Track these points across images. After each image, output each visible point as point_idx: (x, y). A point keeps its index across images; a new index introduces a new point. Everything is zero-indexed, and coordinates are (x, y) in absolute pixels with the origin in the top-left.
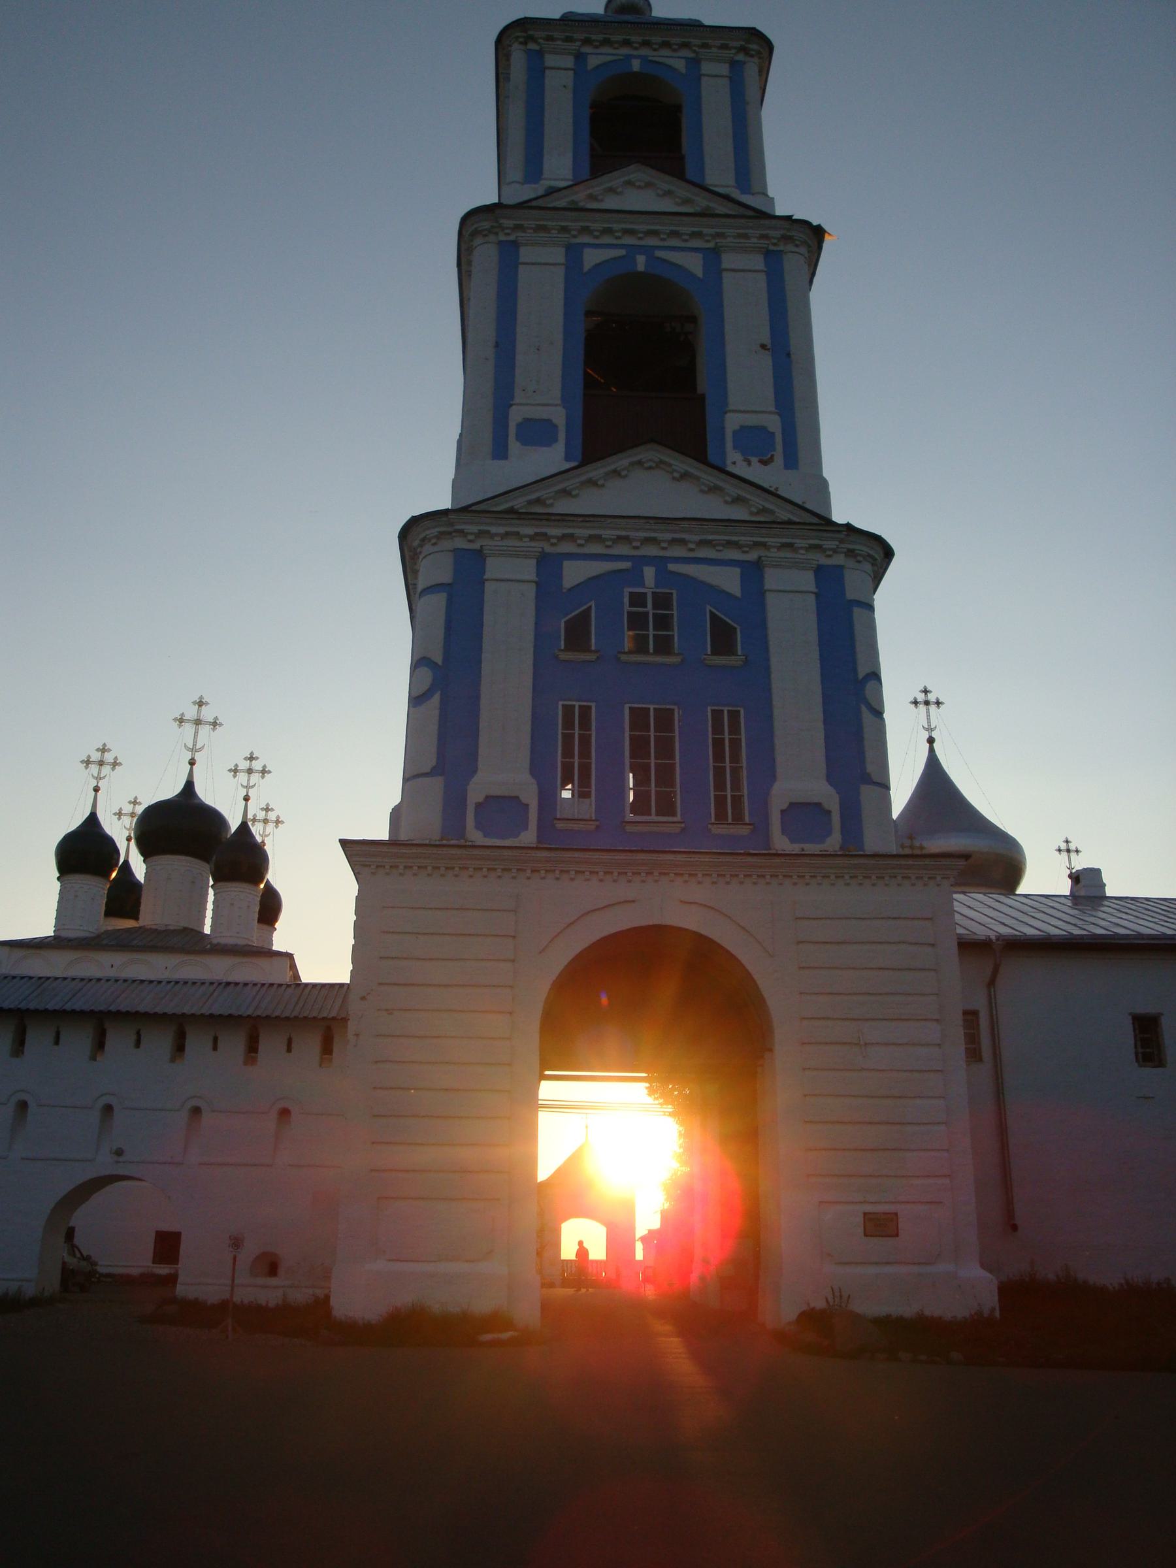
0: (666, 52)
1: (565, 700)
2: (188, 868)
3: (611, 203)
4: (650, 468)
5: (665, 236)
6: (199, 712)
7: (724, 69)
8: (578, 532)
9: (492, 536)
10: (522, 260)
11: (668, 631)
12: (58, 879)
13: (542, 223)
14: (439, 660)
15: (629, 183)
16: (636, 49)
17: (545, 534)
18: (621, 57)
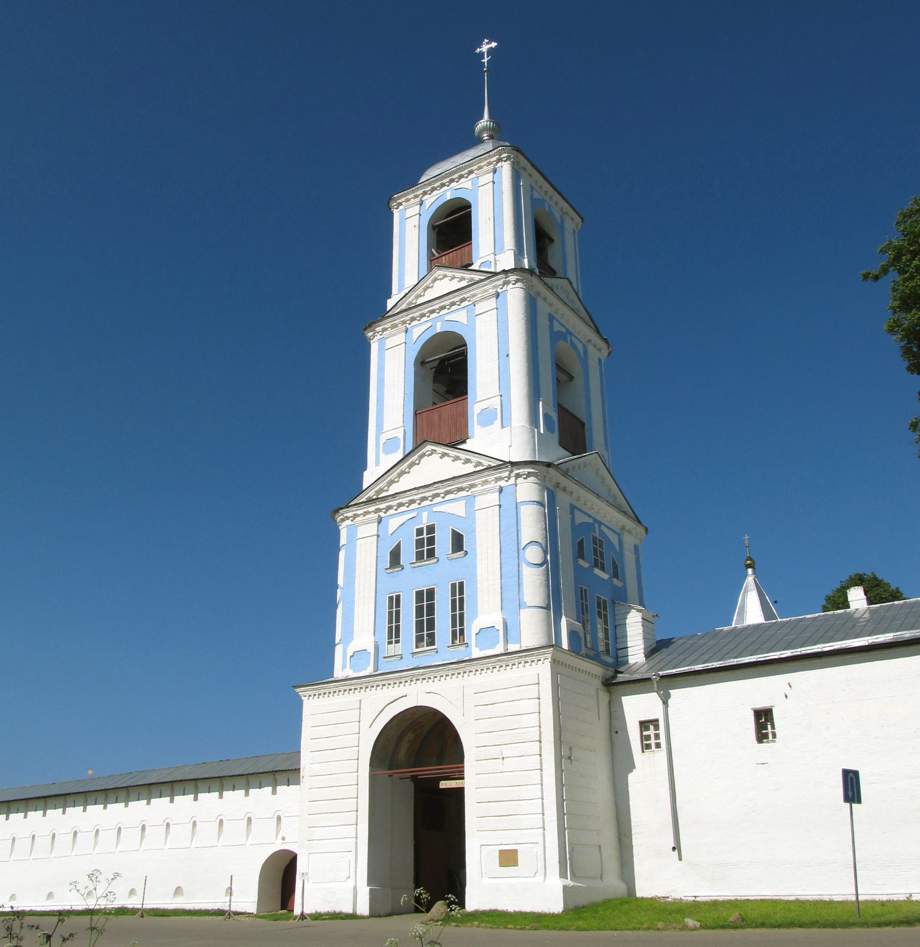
4: (430, 455)
8: (392, 503)
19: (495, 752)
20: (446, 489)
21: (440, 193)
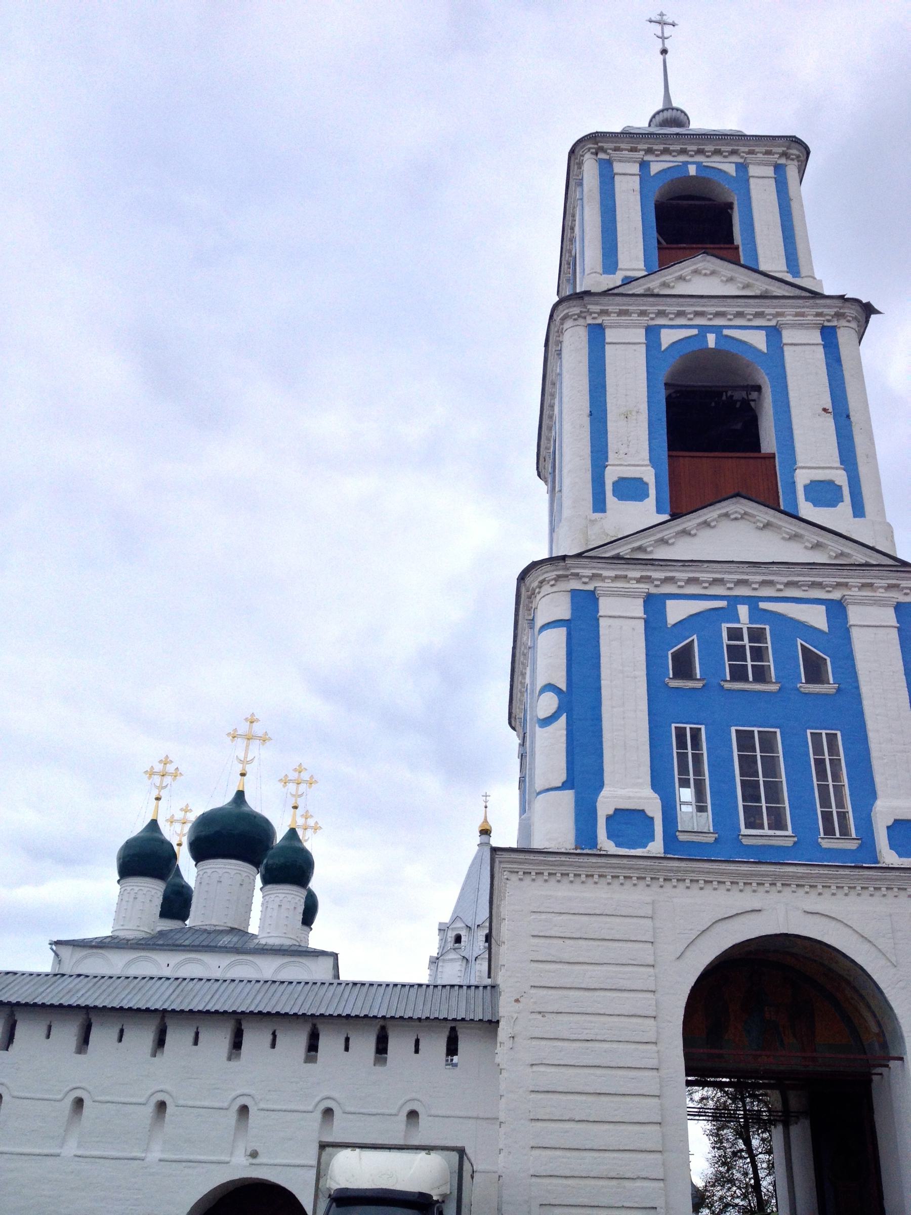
2: (238, 872)
3: (681, 289)
4: (736, 519)
6: (250, 728)
7: (770, 171)
10: (608, 340)
11: (763, 662)
12: (119, 882)
14: (563, 686)
15: (696, 272)
16: (692, 156)
17: (650, 577)
18: (680, 164)
20: (790, 579)
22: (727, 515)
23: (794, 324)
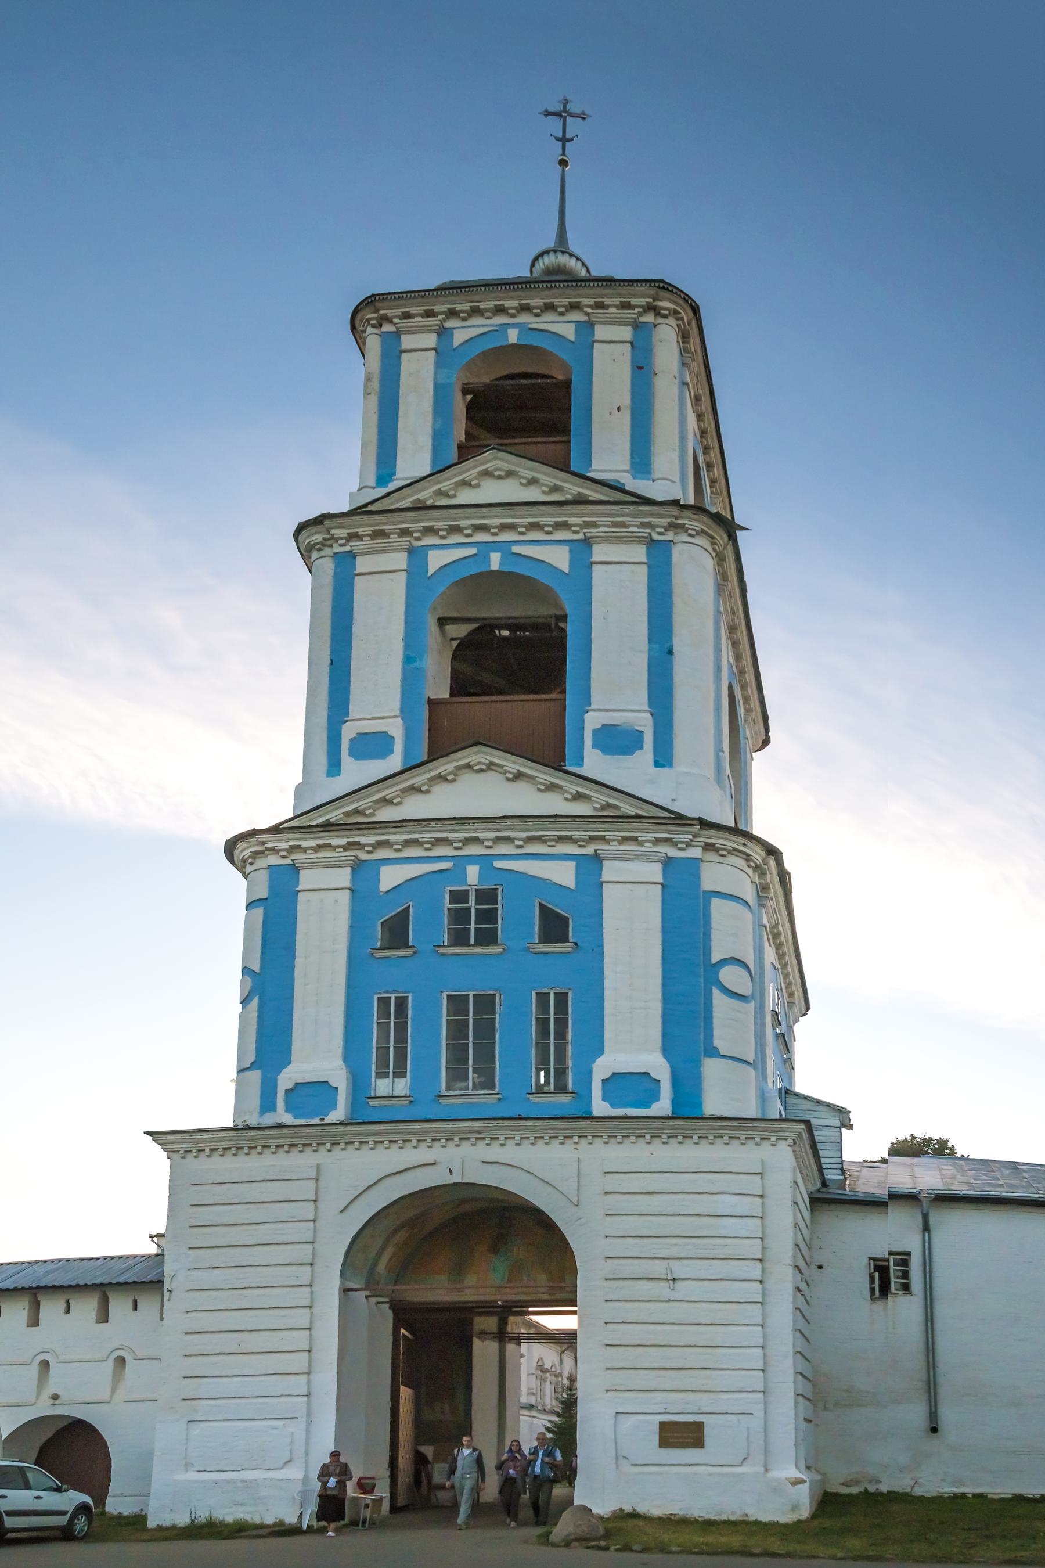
0: (550, 317)
1: (380, 993)
3: (465, 497)
4: (481, 770)
5: (550, 529)
8: (392, 838)
9: (305, 850)
13: (377, 528)
15: (487, 474)
16: (513, 316)
17: (358, 843)
19: (658, 1268)
20: (530, 834)
21: (491, 325)
22: (468, 766)
23: (608, 537)
